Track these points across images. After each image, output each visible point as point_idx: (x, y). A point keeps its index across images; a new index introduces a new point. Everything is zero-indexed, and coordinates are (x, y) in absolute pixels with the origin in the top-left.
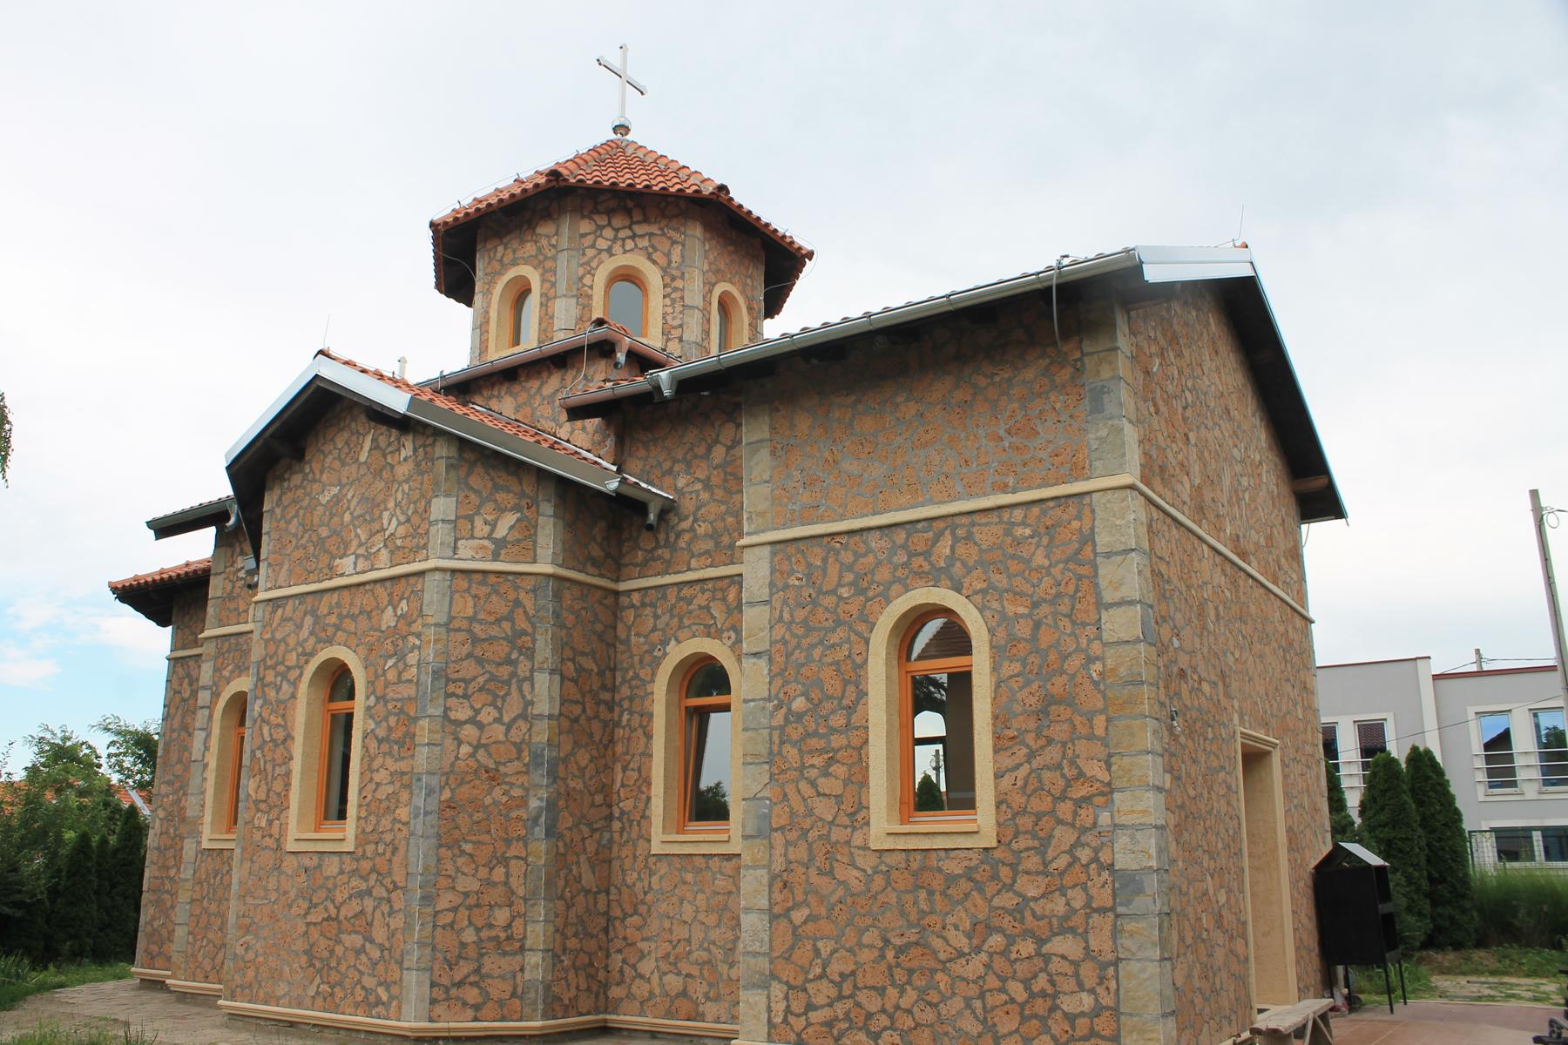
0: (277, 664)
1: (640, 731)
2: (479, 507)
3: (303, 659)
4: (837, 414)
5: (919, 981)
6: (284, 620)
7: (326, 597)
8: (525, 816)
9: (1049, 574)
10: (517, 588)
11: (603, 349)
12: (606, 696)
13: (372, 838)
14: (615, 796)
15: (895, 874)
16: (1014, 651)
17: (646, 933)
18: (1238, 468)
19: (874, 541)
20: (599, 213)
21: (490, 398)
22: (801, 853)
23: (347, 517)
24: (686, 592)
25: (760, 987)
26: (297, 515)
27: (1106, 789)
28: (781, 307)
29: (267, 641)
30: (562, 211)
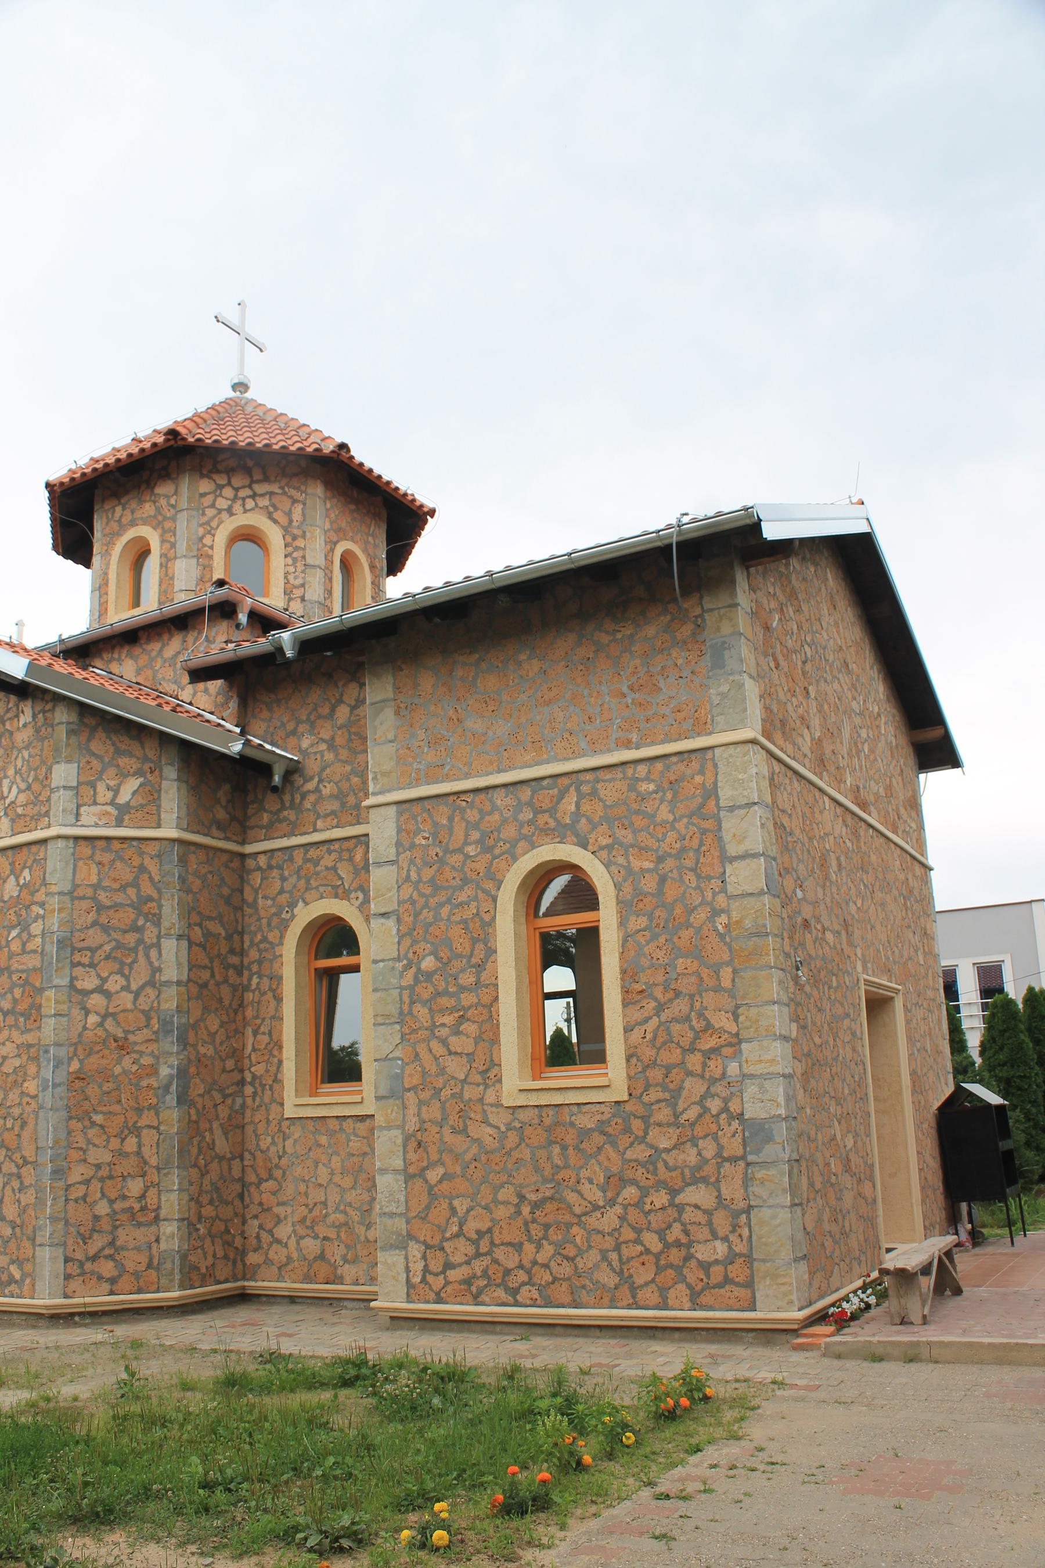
1: (270, 994)
2: (102, 772)
5: (555, 1236)
8: (156, 1085)
9: (673, 828)
10: (141, 854)
11: (225, 610)
12: (234, 960)
14: (247, 1061)
15: (528, 1131)
16: (641, 905)
18: (857, 720)
19: (500, 799)
20: (218, 472)
21: (110, 661)
22: (434, 1112)
24: (313, 853)
25: (397, 1247)
27: (734, 1040)
30: (181, 470)
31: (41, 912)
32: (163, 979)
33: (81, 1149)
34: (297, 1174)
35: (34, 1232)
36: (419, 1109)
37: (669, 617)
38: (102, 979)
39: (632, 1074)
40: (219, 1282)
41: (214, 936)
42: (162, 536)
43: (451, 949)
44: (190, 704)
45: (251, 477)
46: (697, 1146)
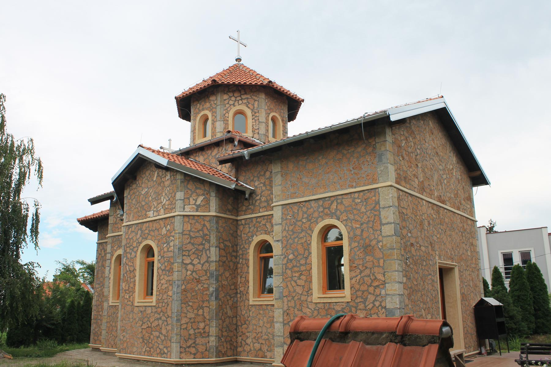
6: (132, 232)
7: (145, 224)
9: (366, 214)
10: (204, 220)
11: (231, 140)
12: (234, 254)
15: (320, 310)
18: (441, 172)
19: (313, 204)
20: (230, 92)
21: (196, 156)
22: (292, 304)
23: (150, 198)
24: (259, 220)
26: (135, 198)
29: (127, 239)
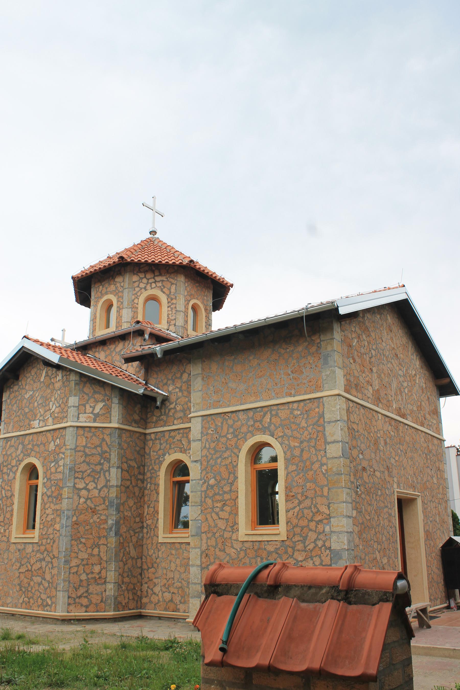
0: (8, 464)
1: (154, 491)
2: (88, 400)
3: (18, 463)
4: (227, 364)
6: (11, 446)
7: (27, 437)
8: (106, 527)
9: (307, 430)
10: (103, 433)
11: (140, 333)
12: (141, 477)
13: (45, 537)
14: (145, 518)
15: (248, 551)
16: (294, 461)
17: (157, 575)
19: (241, 416)
20: (141, 272)
21: (95, 352)
22: (212, 542)
23: (36, 404)
24: (172, 434)
25: (197, 597)
26: (16, 403)
27: (328, 517)
28: (222, 306)
29: (4, 455)
30: (126, 272)
31: (63, 456)
32: (110, 484)
33: (76, 552)
34: (163, 566)
35: (57, 585)
36: (207, 541)
37: (307, 343)
38: (86, 484)
39: (289, 529)
40: (130, 609)
41: (132, 467)
42: (118, 299)
43: (221, 476)
44: (126, 371)
45: (154, 274)
46: (313, 560)
